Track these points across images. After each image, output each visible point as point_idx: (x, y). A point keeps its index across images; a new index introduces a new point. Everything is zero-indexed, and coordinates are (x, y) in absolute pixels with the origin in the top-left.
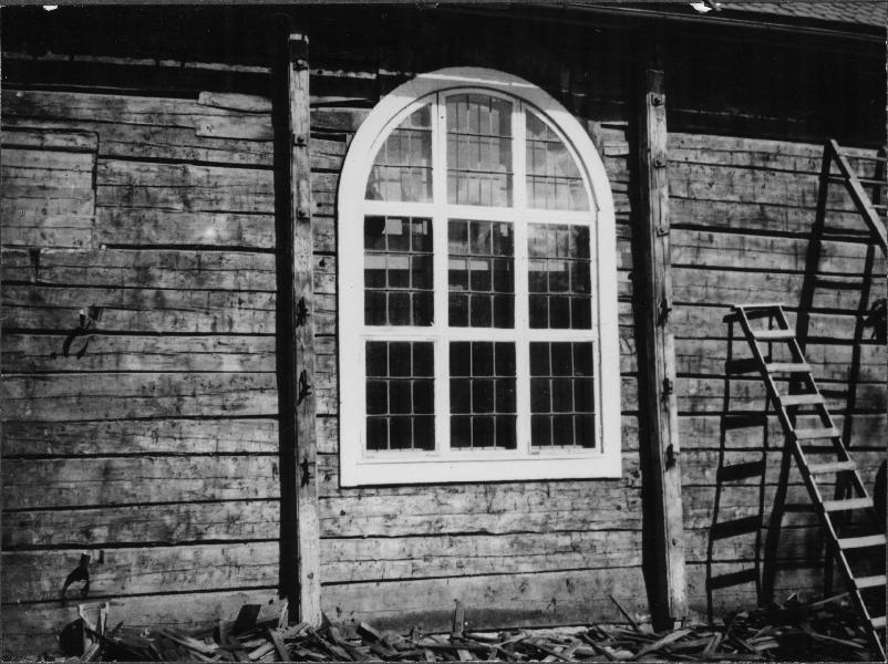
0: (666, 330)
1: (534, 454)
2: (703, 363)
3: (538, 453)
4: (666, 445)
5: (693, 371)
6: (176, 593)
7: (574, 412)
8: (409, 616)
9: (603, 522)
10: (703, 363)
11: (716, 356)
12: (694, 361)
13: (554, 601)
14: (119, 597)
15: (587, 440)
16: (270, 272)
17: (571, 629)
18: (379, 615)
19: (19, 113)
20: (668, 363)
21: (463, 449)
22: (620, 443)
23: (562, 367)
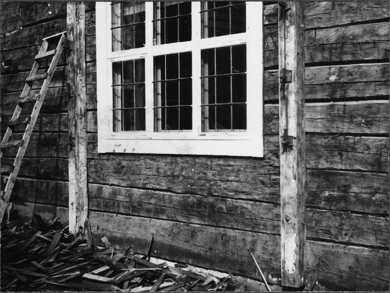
0: (287, 23)
1: (201, 135)
2: (345, 49)
3: (204, 135)
4: (79, 108)
5: (336, 60)
6: (161, 219)
7: (216, 104)
8: (128, 238)
9: (250, 194)
10: (345, 49)
11: (360, 40)
12: (336, 49)
13: (210, 249)
14: (193, 223)
15: (240, 123)
16: (330, 59)
17: (220, 273)
18: (114, 235)
19: (210, 5)
20: (289, 54)
21: (140, 131)
22: (98, 114)
23: (223, 67)
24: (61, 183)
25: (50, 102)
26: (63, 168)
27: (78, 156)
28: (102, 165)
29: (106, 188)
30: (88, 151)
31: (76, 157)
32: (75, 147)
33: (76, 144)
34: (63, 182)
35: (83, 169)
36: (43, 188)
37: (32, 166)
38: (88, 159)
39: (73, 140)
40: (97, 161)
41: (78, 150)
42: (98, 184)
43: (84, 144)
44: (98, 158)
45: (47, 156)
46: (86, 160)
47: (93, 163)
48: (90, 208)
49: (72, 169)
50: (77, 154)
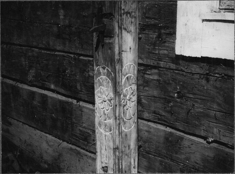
24: (72, 103)
25: (30, 49)
26: (75, 75)
27: (120, 61)
28: (183, 87)
29: (193, 143)
30: (143, 48)
31: (113, 62)
32: (111, 37)
33: (117, 30)
34: (75, 102)
35: (129, 91)
36: (35, 103)
37: (13, 61)
38: (140, 65)
39: (105, 20)
40: (169, 74)
41: (120, 47)
42: (173, 128)
43: (132, 28)
44: (173, 66)
45: (41, 46)
46: (136, 68)
47: (156, 77)
48: (139, 171)
49: (103, 92)
50: (117, 57)
